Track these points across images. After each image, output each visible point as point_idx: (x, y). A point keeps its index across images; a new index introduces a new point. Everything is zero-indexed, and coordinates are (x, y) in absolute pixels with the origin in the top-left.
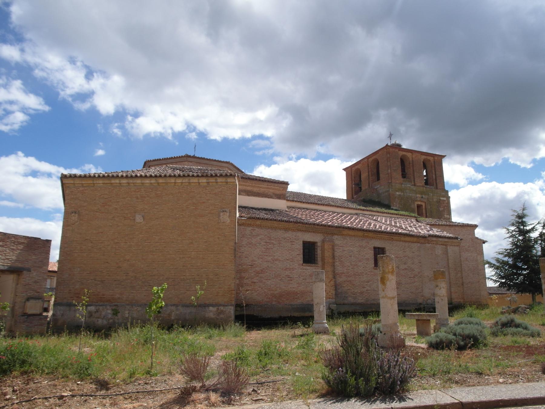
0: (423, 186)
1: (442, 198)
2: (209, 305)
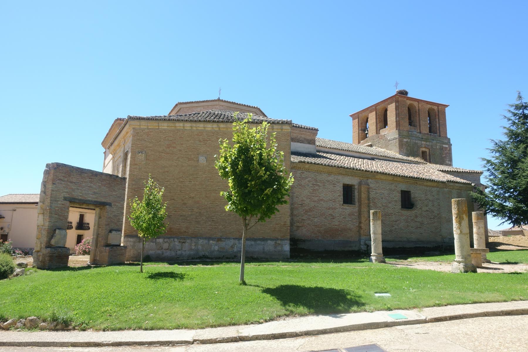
0: (427, 134)
1: (444, 146)
2: (267, 240)
